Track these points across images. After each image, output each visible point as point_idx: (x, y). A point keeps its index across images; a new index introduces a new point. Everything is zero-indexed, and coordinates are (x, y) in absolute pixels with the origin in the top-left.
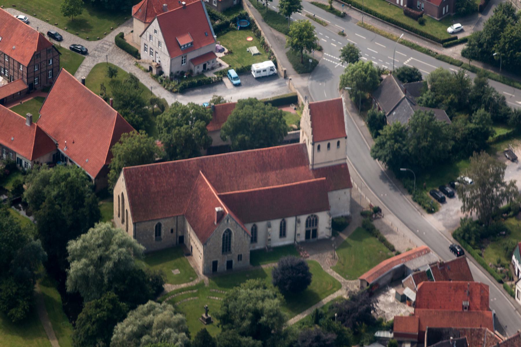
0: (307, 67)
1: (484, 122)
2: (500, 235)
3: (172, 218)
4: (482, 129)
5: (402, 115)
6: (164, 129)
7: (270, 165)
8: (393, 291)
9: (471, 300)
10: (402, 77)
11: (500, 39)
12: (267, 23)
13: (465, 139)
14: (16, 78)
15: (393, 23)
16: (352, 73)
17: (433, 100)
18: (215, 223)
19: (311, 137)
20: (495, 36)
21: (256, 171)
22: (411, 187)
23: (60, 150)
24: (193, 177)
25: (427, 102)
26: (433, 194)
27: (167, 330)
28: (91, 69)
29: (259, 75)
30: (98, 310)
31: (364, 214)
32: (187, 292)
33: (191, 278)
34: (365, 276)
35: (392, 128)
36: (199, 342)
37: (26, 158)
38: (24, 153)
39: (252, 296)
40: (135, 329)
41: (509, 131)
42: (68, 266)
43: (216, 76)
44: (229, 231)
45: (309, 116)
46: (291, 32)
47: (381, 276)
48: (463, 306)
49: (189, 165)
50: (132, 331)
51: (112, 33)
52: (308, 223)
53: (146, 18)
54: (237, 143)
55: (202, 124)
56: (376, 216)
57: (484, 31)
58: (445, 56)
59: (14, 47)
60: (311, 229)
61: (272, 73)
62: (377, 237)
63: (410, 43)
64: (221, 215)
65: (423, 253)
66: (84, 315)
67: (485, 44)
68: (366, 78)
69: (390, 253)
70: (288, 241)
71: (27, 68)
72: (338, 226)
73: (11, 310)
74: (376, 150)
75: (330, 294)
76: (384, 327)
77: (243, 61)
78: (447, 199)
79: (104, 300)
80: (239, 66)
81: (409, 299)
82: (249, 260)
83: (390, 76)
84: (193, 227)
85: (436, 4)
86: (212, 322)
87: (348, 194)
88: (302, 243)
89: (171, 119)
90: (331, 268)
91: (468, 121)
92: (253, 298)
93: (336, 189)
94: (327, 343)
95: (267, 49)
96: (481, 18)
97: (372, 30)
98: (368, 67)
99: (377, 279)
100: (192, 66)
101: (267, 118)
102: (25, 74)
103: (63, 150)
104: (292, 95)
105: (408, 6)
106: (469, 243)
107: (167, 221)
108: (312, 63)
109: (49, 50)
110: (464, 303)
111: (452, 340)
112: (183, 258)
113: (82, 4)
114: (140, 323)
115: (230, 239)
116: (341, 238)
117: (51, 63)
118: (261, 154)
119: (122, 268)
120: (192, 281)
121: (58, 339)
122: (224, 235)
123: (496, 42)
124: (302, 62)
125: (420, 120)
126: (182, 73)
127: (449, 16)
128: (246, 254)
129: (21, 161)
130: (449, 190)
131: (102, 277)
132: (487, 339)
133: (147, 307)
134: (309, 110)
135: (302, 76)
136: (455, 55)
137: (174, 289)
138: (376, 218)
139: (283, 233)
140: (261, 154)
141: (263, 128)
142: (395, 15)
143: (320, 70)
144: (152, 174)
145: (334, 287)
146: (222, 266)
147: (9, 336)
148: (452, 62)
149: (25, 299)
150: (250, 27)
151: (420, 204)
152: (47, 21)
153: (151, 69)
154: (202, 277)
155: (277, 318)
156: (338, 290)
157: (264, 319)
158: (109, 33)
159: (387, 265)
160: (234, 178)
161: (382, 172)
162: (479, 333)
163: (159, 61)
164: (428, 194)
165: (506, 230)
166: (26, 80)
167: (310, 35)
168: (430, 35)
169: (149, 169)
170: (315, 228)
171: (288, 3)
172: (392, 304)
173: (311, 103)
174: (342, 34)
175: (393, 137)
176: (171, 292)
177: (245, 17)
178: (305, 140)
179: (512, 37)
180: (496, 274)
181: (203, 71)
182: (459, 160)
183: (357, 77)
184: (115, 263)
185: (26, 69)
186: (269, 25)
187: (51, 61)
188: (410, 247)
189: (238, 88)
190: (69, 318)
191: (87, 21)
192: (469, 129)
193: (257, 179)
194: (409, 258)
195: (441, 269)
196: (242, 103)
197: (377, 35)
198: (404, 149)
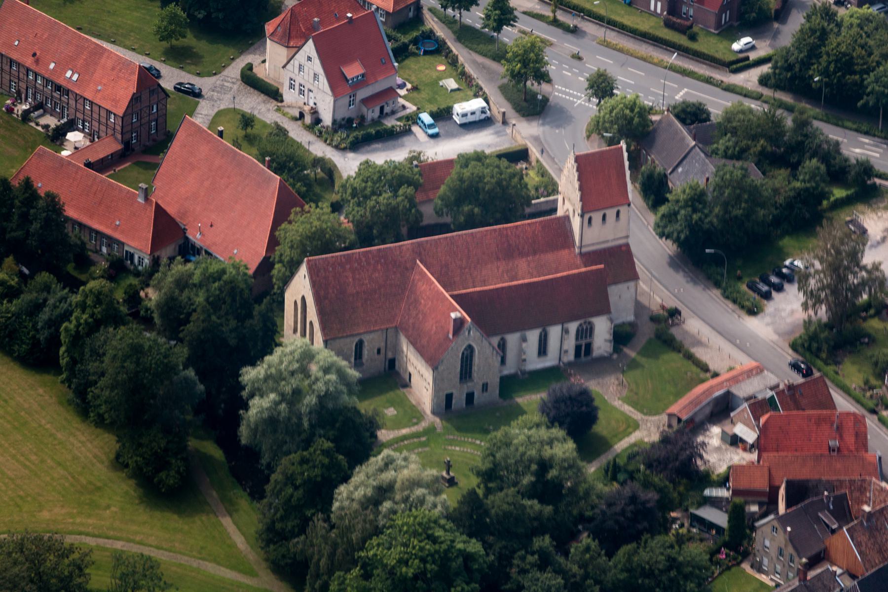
0: (534, 107)
1: (818, 178)
2: (862, 344)
3: (380, 332)
4: (814, 189)
5: (694, 172)
6: (352, 201)
7: (518, 249)
8: (716, 430)
9: (841, 438)
10: (683, 116)
11: (821, 57)
12: (463, 44)
13: (790, 205)
14: (102, 134)
15: (650, 39)
16: (611, 112)
17: (735, 148)
18: (451, 336)
19: (578, 206)
20: (813, 53)
21: (498, 259)
22: (719, 278)
23: (191, 237)
24: (407, 269)
25: (725, 151)
26: (752, 287)
27: (419, 492)
28: (211, 118)
29: (465, 120)
30: (305, 467)
31: (654, 319)
32: (412, 441)
33: (415, 421)
34: (674, 409)
35: (687, 191)
36: (466, 509)
37: (141, 251)
38: (139, 244)
39: (532, 440)
40: (369, 492)
41: (849, 192)
42: (246, 407)
43: (399, 123)
44: (470, 348)
45: (576, 175)
46: (510, 54)
47: (698, 408)
48: (829, 448)
49: (401, 252)
50: (365, 496)
51: (234, 64)
52: (580, 334)
53: (292, 38)
54: (462, 219)
55: (410, 190)
56: (673, 321)
57: (793, 46)
58: (735, 86)
59: (99, 88)
60: (583, 342)
61: (483, 116)
62: (679, 351)
63: (680, 67)
64: (459, 324)
65: (754, 372)
66: (280, 476)
67: (797, 66)
68: (632, 119)
69: (702, 375)
70: (550, 361)
71: (122, 118)
72: (622, 337)
73: (161, 474)
74: (661, 224)
75: (624, 437)
76: (714, 482)
77: (436, 99)
78: (774, 294)
79: (315, 451)
80: (435, 109)
81: (742, 441)
82: (498, 392)
83: (668, 115)
84: (414, 343)
85: (711, 9)
86: (457, 483)
87: (633, 290)
88: (570, 364)
89: (364, 185)
90: (619, 399)
91: (791, 179)
92: (535, 443)
93: (615, 282)
94: (648, 505)
95: (470, 82)
96: (778, 28)
97: (621, 50)
98: (635, 103)
99: (691, 414)
100: (364, 110)
101: (505, 180)
102: (119, 128)
103: (195, 237)
104: (520, 148)
105: (669, 13)
106: (818, 357)
107: (372, 336)
108: (541, 101)
109: (153, 90)
110: (831, 443)
111: (827, 496)
112: (398, 392)
113: (186, 23)
114: (375, 484)
115: (471, 360)
116: (626, 355)
117: (155, 110)
118: (505, 232)
119: (330, 405)
120: (416, 424)
121: (231, 516)
122: (463, 354)
123: (814, 61)
124: (525, 100)
125: (728, 176)
126: (350, 121)
127: (731, 26)
128: (495, 383)
129: (132, 256)
130: (774, 279)
131: (300, 418)
132: (874, 494)
133: (383, 459)
134: (575, 165)
135: (528, 120)
136: (749, 83)
137: (391, 436)
138: (673, 325)
139: (543, 350)
140: (505, 232)
141: (496, 196)
142: (651, 27)
143: (566, 110)
144: (348, 266)
145: (629, 426)
146: (459, 400)
147: (158, 514)
148: (747, 95)
149: (179, 457)
150: (439, 49)
151: (735, 301)
152: (134, 50)
153: (302, 115)
154: (430, 419)
155: (575, 470)
156: (635, 430)
157: (553, 473)
158: (229, 65)
159: (704, 392)
160: (467, 270)
161: (670, 257)
162: (861, 486)
163: (315, 104)
164: (744, 287)
165: (869, 336)
166: (119, 137)
167: (539, 60)
168: (708, 56)
169: (343, 260)
170: (588, 340)
171: (497, 12)
172: (718, 449)
173: (577, 154)
174: (578, 57)
175: (690, 203)
176: (388, 442)
177: (430, 35)
178: (568, 210)
179: (840, 53)
180: (865, 401)
181: (379, 117)
182: (782, 236)
183: (618, 118)
184: (319, 397)
185: (120, 120)
186: (467, 47)
187: (155, 107)
188: (732, 365)
189: (436, 140)
190: (241, 485)
191: (192, 48)
192: (794, 189)
193: (500, 270)
194: (735, 380)
195: (791, 396)
196: (465, 160)
197: (629, 57)
198: (707, 220)
